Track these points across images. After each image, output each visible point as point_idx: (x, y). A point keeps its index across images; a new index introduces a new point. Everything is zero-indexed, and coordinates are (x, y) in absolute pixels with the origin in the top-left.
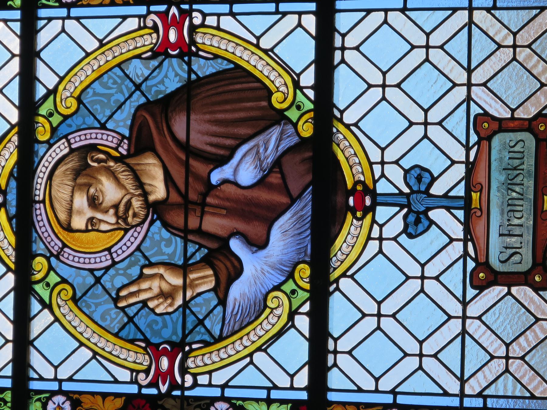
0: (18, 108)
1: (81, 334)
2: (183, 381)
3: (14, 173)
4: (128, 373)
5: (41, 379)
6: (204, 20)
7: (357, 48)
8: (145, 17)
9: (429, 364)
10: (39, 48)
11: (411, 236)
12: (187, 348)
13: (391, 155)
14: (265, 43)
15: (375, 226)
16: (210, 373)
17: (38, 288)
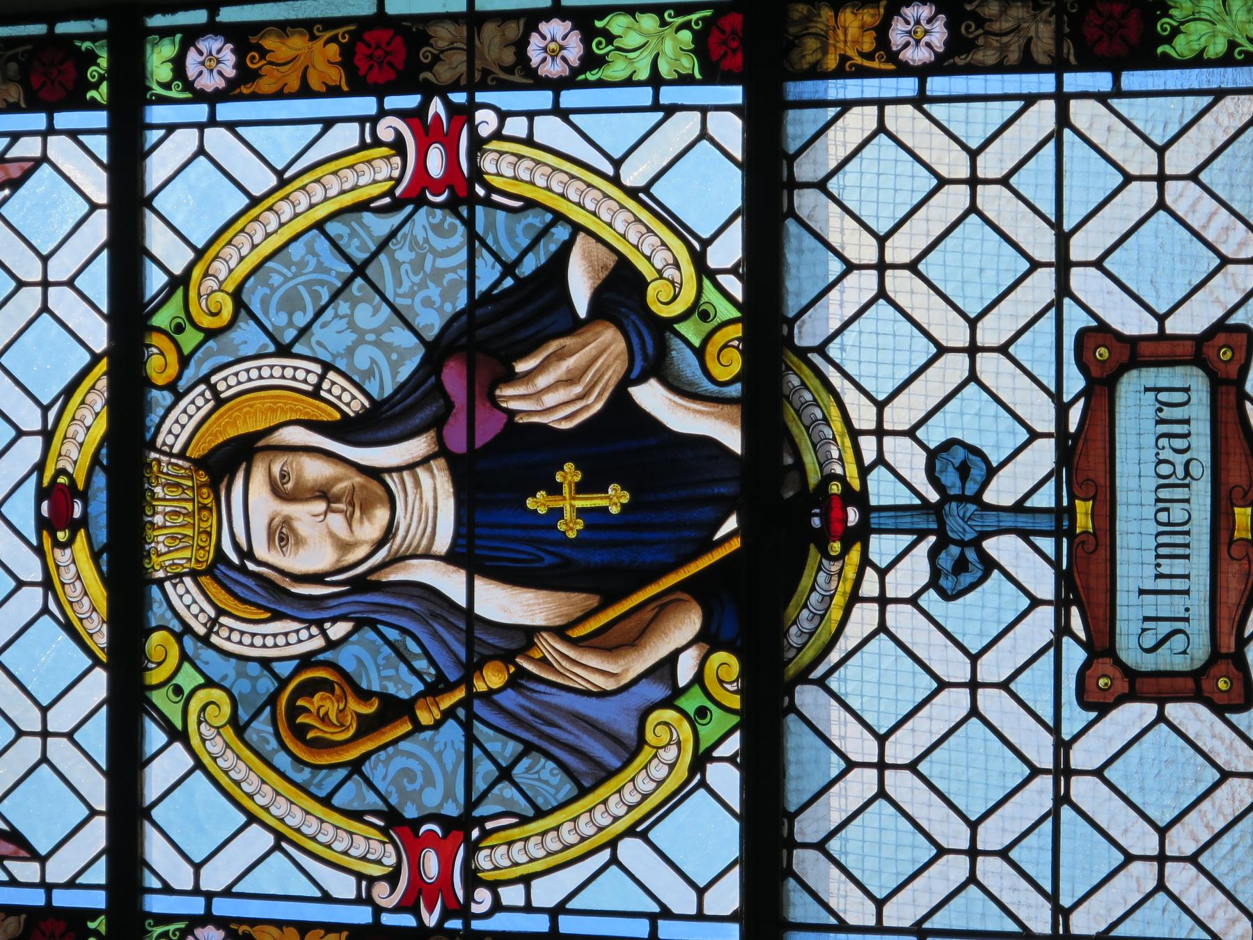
0: (474, 302)
1: (251, 796)
2: (469, 897)
3: (100, 457)
4: (352, 880)
5: (167, 889)
6: (501, 124)
7: (942, 182)
8: (374, 120)
9: (990, 869)
10: (150, 187)
11: (947, 596)
12: (475, 833)
13: (897, 417)
14: (633, 175)
15: (869, 572)
16: (526, 880)
17: (158, 698)
